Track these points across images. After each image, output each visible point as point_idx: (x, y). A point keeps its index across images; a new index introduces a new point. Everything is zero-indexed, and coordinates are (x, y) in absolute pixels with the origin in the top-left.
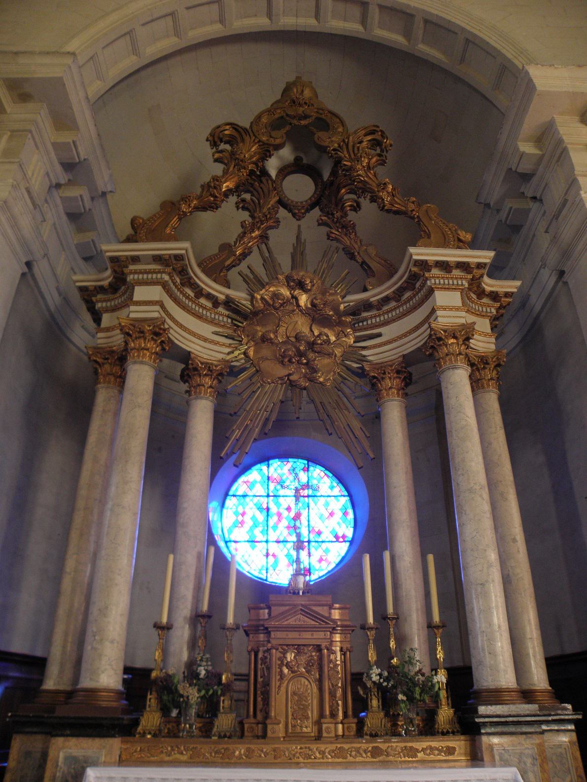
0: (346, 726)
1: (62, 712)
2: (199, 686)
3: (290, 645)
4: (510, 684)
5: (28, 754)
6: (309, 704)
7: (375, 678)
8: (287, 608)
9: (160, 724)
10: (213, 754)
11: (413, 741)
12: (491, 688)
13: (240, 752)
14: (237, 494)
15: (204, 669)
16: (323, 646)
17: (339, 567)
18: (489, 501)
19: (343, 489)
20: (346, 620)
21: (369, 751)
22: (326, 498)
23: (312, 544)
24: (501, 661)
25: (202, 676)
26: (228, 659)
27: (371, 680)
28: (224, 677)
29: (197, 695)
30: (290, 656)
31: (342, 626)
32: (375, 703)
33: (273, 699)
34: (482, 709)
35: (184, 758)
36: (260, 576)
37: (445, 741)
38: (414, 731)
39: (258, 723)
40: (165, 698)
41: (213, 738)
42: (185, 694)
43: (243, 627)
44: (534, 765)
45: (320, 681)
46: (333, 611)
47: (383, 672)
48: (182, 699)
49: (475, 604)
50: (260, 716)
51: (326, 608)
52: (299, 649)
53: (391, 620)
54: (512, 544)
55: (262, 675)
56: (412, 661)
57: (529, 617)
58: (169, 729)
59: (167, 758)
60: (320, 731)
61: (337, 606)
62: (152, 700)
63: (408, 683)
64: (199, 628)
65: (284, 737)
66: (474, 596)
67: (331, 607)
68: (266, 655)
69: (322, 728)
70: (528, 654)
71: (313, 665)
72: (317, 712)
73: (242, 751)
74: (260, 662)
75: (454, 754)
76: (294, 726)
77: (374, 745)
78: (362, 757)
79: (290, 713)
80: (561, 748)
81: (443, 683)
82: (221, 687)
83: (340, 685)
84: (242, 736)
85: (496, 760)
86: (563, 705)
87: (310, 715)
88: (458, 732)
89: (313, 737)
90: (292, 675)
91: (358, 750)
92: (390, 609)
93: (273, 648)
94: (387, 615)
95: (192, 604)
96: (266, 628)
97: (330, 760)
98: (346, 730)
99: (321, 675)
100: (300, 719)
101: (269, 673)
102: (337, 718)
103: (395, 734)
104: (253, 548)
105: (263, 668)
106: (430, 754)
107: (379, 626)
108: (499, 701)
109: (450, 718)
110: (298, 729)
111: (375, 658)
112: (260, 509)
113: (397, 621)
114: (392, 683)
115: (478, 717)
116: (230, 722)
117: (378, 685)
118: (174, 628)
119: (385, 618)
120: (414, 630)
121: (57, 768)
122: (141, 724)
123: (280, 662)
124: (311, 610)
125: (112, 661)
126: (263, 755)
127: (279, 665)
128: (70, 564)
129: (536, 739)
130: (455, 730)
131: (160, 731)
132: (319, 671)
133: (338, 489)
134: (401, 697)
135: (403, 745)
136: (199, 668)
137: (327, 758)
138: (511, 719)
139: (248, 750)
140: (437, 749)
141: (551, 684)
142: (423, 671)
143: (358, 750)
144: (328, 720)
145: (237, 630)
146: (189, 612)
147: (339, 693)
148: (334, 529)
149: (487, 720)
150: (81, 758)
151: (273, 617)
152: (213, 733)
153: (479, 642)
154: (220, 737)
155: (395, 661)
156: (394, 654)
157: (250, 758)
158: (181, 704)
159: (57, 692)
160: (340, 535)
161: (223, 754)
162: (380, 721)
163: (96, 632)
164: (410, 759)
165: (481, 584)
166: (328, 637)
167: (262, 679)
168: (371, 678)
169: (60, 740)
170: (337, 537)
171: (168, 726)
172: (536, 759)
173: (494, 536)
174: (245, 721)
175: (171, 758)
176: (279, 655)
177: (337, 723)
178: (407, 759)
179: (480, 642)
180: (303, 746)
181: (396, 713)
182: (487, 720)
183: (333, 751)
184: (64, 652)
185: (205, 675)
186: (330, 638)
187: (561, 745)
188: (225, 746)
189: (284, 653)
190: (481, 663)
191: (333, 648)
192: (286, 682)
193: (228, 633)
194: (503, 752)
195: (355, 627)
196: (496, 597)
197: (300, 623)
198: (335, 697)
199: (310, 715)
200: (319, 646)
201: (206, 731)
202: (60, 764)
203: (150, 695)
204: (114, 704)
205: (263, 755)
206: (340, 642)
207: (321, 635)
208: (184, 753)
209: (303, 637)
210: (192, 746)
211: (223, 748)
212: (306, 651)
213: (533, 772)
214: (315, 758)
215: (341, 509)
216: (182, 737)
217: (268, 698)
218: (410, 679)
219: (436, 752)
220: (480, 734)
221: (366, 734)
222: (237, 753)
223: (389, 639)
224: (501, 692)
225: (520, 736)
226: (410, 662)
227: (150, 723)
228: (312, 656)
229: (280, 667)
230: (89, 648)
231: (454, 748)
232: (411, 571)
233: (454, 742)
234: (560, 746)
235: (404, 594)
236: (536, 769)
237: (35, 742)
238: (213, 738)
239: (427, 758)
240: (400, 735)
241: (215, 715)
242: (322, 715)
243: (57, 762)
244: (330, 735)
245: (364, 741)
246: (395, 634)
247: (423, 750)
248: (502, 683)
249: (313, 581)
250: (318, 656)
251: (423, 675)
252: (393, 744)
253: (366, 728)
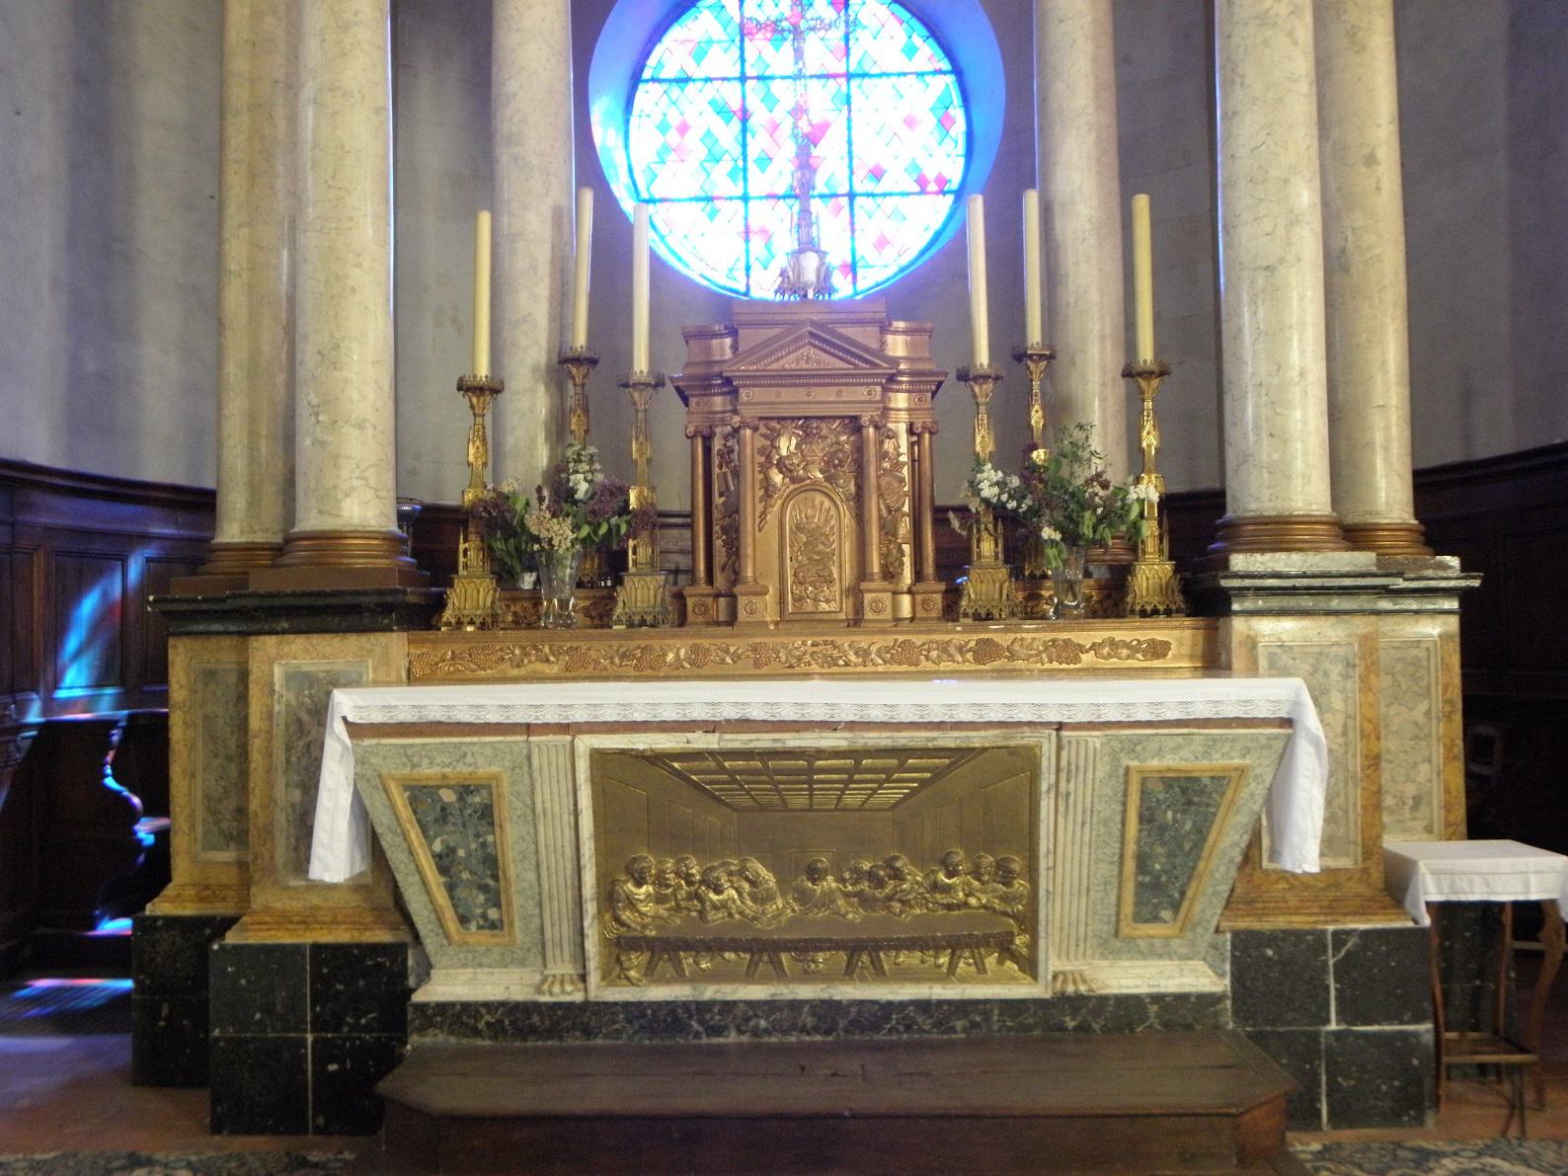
0: (919, 598)
1: (263, 582)
2: (575, 516)
3: (784, 419)
4: (1314, 507)
5: (210, 675)
6: (834, 550)
7: (989, 492)
8: (777, 331)
9: (493, 603)
10: (617, 660)
11: (1073, 630)
12: (1266, 514)
13: (677, 654)
14: (661, 76)
15: (585, 480)
16: (865, 419)
17: (927, 257)
18: (1311, 48)
19: (940, 53)
20: (921, 360)
21: (969, 650)
22: (893, 79)
23: (858, 201)
24: (1299, 455)
25: (580, 495)
26: (641, 455)
27: (979, 495)
28: (633, 496)
29: (572, 536)
30: (786, 445)
31: (911, 374)
32: (987, 547)
33: (750, 541)
34: (1239, 562)
35: (555, 669)
36: (730, 284)
37: (1146, 629)
38: (1077, 607)
39: (718, 596)
40: (499, 545)
41: (615, 627)
42: (544, 534)
43: (672, 379)
44: (1346, 677)
45: (859, 499)
46: (890, 338)
47: (1008, 479)
48: (536, 547)
49: (1246, 321)
50: (720, 580)
51: (873, 330)
52: (808, 426)
53: (1036, 362)
54: (1363, 169)
55: (723, 489)
56: (1080, 453)
57: (1383, 354)
58: (515, 614)
59: (515, 672)
60: (859, 609)
61: (900, 325)
62: (469, 551)
63: (1068, 504)
64: (571, 389)
65: (777, 623)
66: (1246, 298)
67: (884, 329)
68: (729, 444)
69: (862, 603)
70: (1370, 444)
71: (841, 464)
72: (852, 567)
73: (682, 652)
74: (716, 461)
75: (1165, 655)
76: (798, 599)
77: (982, 636)
78: (954, 661)
79: (789, 572)
80: (1418, 647)
81: (1151, 505)
82: (627, 517)
83: (906, 509)
84: (682, 621)
85: (1260, 668)
86: (1438, 557)
87: (836, 576)
88: (1179, 611)
89: (843, 621)
90: (792, 487)
91: (944, 648)
92: (1035, 335)
93: (744, 425)
94: (1026, 348)
95: (550, 332)
96: (728, 381)
97: (880, 669)
98: (919, 607)
99: (859, 487)
100: (812, 584)
101: (738, 486)
102: (898, 582)
103: (1030, 611)
104: (713, 215)
105: (725, 474)
106: (1109, 656)
107: (1004, 373)
108: (1288, 542)
109: (1164, 582)
110: (809, 606)
111: (991, 448)
112: (722, 110)
113: (1049, 365)
114: (1030, 503)
115: (1225, 577)
116: (652, 592)
117: (998, 510)
118: (504, 393)
119: (1021, 356)
120: (1090, 385)
121: (272, 696)
122: (450, 605)
123: (763, 459)
124: (833, 333)
125: (366, 470)
126: (728, 660)
127: (761, 465)
128: (236, 251)
129: (1361, 625)
130: (1174, 607)
131: (494, 616)
132: (856, 478)
133: (928, 54)
134: (1048, 533)
135: (1048, 636)
136: (572, 477)
137: (877, 665)
138: (1305, 582)
139: (695, 649)
140: (1127, 645)
141: (1417, 514)
142: (1107, 476)
143: (944, 648)
144: (878, 584)
145: (660, 389)
146: (544, 354)
147: (905, 527)
148: (915, 165)
149: (1247, 582)
150: (321, 676)
151: (744, 352)
152: (615, 618)
153: (1248, 410)
154: (631, 625)
155: (1039, 455)
156: (1040, 442)
157: (699, 667)
158: (538, 557)
159: (250, 548)
160: (931, 175)
161: (638, 660)
162: (997, 585)
163: (318, 406)
164: (1064, 666)
165: (1267, 268)
166: (878, 398)
167: (723, 499)
168: (977, 492)
169: (270, 641)
170: (922, 182)
171: (513, 608)
172: (1354, 666)
173: (1315, 144)
174: (687, 591)
175: (522, 672)
176: (760, 442)
177: (895, 593)
178: (1055, 665)
179: (1250, 411)
180: (819, 639)
181: (1038, 573)
182: (1247, 582)
183: (888, 650)
184: (253, 458)
185: (587, 492)
186: (882, 401)
187: (1420, 641)
188: (643, 643)
189: (773, 437)
190: (1245, 457)
191: (890, 425)
192: (779, 502)
193: (636, 395)
194: (1279, 651)
195: (946, 375)
196: (1302, 298)
197: (807, 367)
198: (895, 535)
199: (836, 576)
200: (855, 419)
201: (601, 615)
202: (277, 688)
203: (465, 541)
204: (383, 563)
205: (728, 660)
206: (909, 410)
207: (861, 393)
208: (552, 659)
209: (818, 399)
210: (568, 645)
211: (638, 647)
212: (824, 432)
213: (1343, 691)
214: (847, 665)
215: (932, 110)
216: (546, 627)
217: (737, 530)
218: (1073, 495)
219: (1125, 652)
220: (1227, 612)
221: (966, 615)
222: (671, 656)
223: (1029, 407)
224: (1287, 523)
225: (1323, 618)
226: (1075, 454)
227: (469, 601)
228: (838, 443)
229: (765, 469)
230: (308, 442)
231: (1166, 645)
232: (1092, 241)
233: (1168, 632)
234: (1417, 643)
235: (1072, 300)
236: (1349, 684)
237: (220, 652)
238: (615, 627)
239: (1102, 663)
240: (1044, 617)
241: (619, 582)
242: (862, 573)
243: (272, 684)
244: (882, 617)
245: (959, 629)
246: (1043, 397)
247: (1094, 647)
248: (1293, 505)
249: (862, 293)
250: (853, 444)
251: (1105, 486)
252: (1024, 635)
253: (964, 603)
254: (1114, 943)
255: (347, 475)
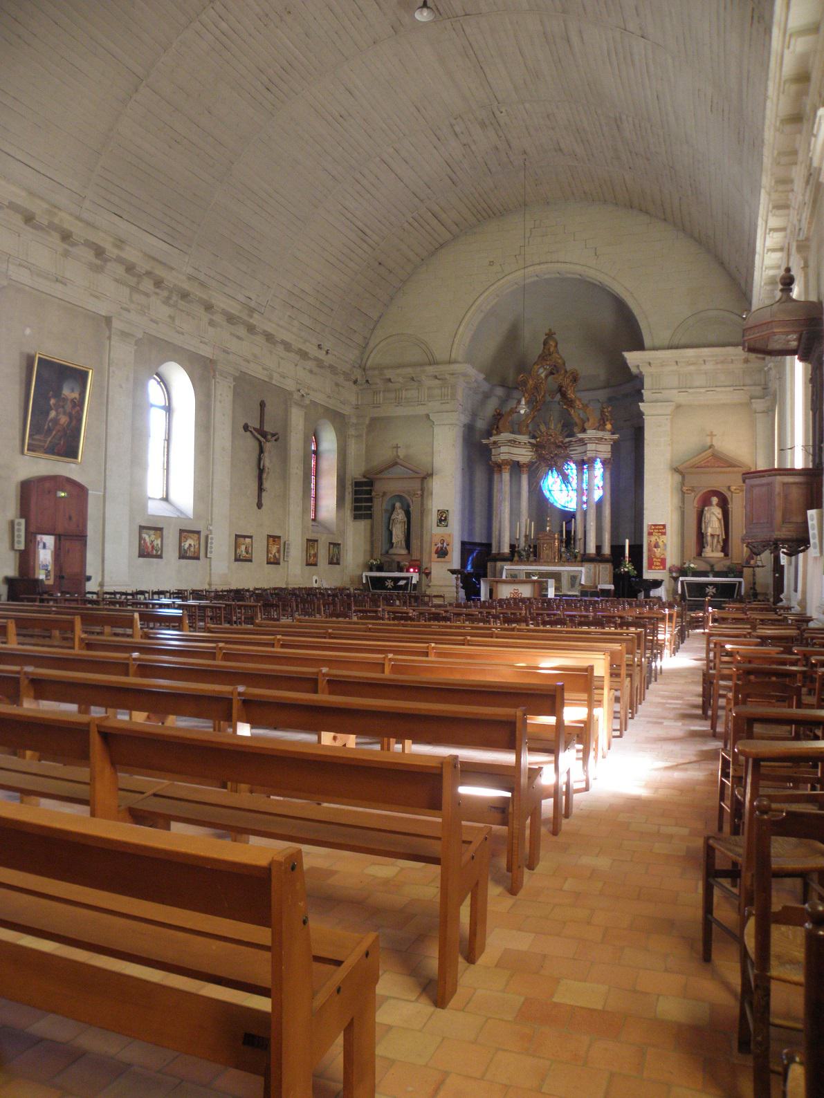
30: (545, 545)
62: (516, 554)
201: (528, 561)
254: (569, 590)
255: (505, 548)
